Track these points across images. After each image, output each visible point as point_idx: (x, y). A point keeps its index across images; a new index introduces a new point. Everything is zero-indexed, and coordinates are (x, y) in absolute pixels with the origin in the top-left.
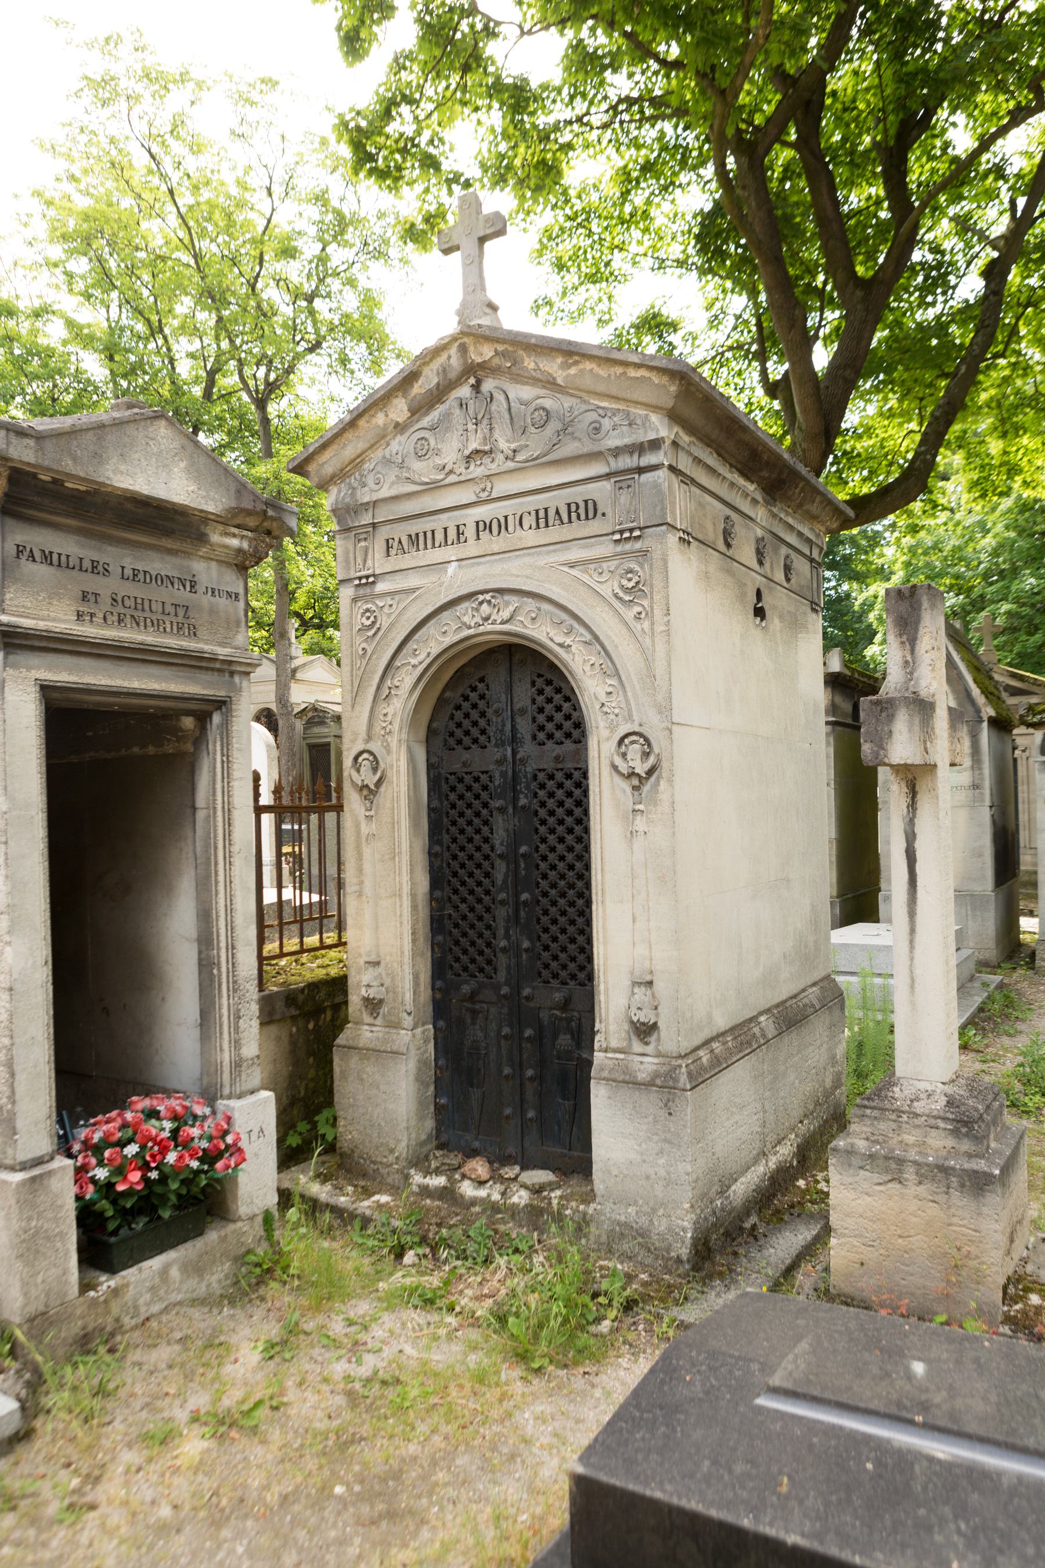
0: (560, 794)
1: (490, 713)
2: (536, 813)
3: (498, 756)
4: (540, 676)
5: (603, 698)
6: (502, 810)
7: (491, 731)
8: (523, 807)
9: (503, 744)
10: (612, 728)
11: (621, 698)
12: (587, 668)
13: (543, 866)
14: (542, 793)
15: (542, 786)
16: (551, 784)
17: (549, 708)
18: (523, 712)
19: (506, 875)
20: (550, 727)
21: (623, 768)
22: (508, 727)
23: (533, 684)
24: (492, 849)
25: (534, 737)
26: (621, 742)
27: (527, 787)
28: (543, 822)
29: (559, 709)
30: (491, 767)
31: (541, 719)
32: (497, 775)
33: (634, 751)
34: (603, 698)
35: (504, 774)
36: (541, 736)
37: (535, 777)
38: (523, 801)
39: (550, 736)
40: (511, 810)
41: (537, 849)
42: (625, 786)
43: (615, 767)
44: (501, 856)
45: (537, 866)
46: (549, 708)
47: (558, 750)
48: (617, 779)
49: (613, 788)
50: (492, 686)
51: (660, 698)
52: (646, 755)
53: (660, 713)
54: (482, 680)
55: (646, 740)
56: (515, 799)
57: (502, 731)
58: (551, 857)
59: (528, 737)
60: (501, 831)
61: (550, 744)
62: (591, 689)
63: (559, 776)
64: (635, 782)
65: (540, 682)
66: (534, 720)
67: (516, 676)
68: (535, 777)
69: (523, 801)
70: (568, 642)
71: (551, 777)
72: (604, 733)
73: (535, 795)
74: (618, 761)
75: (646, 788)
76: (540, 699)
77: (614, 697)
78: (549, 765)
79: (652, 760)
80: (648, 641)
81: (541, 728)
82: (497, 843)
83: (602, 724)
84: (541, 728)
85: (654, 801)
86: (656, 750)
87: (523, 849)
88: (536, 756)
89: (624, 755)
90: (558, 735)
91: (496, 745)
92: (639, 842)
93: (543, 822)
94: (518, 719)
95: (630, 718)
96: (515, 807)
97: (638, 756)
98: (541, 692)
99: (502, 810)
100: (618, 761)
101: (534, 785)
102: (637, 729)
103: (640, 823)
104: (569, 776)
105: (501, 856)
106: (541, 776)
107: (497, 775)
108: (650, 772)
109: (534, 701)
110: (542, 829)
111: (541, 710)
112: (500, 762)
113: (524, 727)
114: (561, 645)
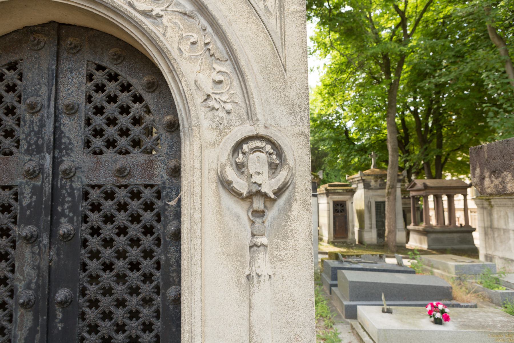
0: (122, 218)
1: (21, 109)
2: (85, 242)
3: (30, 166)
4: (100, 68)
5: (208, 88)
6: (31, 240)
7: (21, 133)
8: (66, 236)
9: (39, 150)
10: (221, 129)
11: (236, 89)
12: (186, 47)
13: (92, 314)
14: (95, 217)
15: (96, 207)
16: (108, 205)
17: (111, 109)
18: (72, 110)
19: (32, 331)
20: (111, 131)
21: (241, 185)
22: (49, 128)
23: (90, 77)
24: (12, 293)
25: (87, 144)
26: (238, 147)
27: (73, 208)
28: (95, 255)
29: (125, 110)
30: (18, 181)
31: (99, 121)
32: (27, 191)
33: (258, 162)
34: (208, 88)
35: (37, 191)
36: (98, 143)
37: (86, 196)
38: (65, 227)
39: (111, 144)
40: (45, 239)
41: (83, 292)
42: (240, 209)
43: (226, 184)
44: (25, 305)
45: (83, 316)
46: (111, 109)
47: (122, 161)
48: (228, 200)
49: (220, 212)
50: (28, 75)
51: (292, 93)
52: (274, 168)
53: (292, 113)
54: (12, 66)
55: (276, 147)
56: (53, 225)
57: (39, 134)
58: (105, 302)
59: (78, 143)
60: (27, 269)
61: (110, 154)
62: (192, 73)
63: (122, 195)
64: (258, 204)
65: (99, 77)
66: (88, 122)
67: (65, 66)
68: (86, 196)
69: (65, 227)
70: (157, 10)
71: (110, 196)
72: (209, 135)
73: (85, 219)
74: (231, 174)
75: (272, 214)
76: (99, 98)
77: (223, 89)
78: (107, 179)
79: (282, 175)
80: (273, 24)
81: (98, 133)
82: (20, 286)
83: (205, 124)
84: (98, 133)
85: (284, 233)
86: (290, 161)
87: (62, 294)
88: (91, 169)
89: (240, 167)
90: (123, 142)
91: (28, 152)
92: (262, 294)
93: (95, 255)
94: (65, 120)
95: (250, 115)
96: (51, 236)
97: (265, 169)
98: (100, 88)
99: (31, 240)
100: (231, 174)
101: (83, 206)
102: (262, 132)
103: (263, 264)
104: (136, 195)
105: (25, 305)
106: (95, 195)
107: (27, 191)
108: (279, 192)
109: (89, 99)
110: (93, 265)
111: (99, 110)
112: (31, 174)
113: (73, 129)
114: (146, 14)
